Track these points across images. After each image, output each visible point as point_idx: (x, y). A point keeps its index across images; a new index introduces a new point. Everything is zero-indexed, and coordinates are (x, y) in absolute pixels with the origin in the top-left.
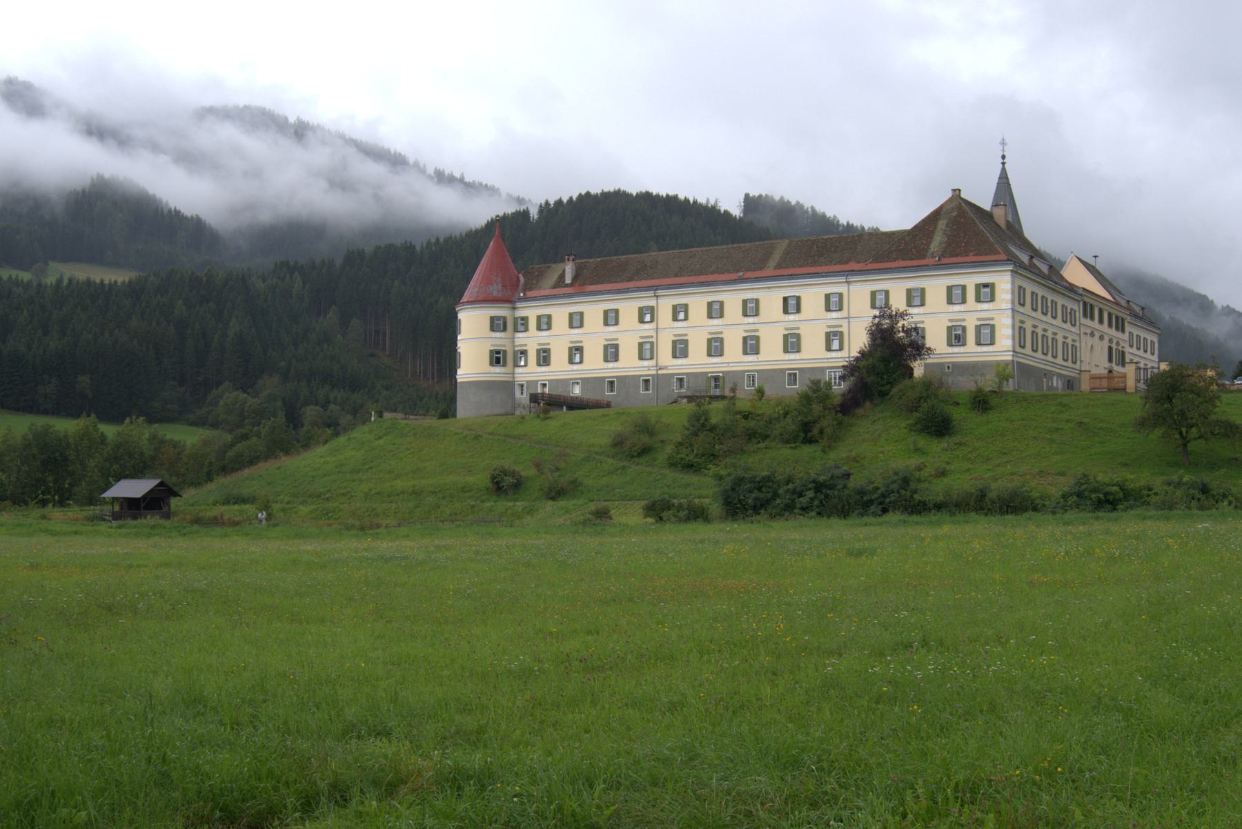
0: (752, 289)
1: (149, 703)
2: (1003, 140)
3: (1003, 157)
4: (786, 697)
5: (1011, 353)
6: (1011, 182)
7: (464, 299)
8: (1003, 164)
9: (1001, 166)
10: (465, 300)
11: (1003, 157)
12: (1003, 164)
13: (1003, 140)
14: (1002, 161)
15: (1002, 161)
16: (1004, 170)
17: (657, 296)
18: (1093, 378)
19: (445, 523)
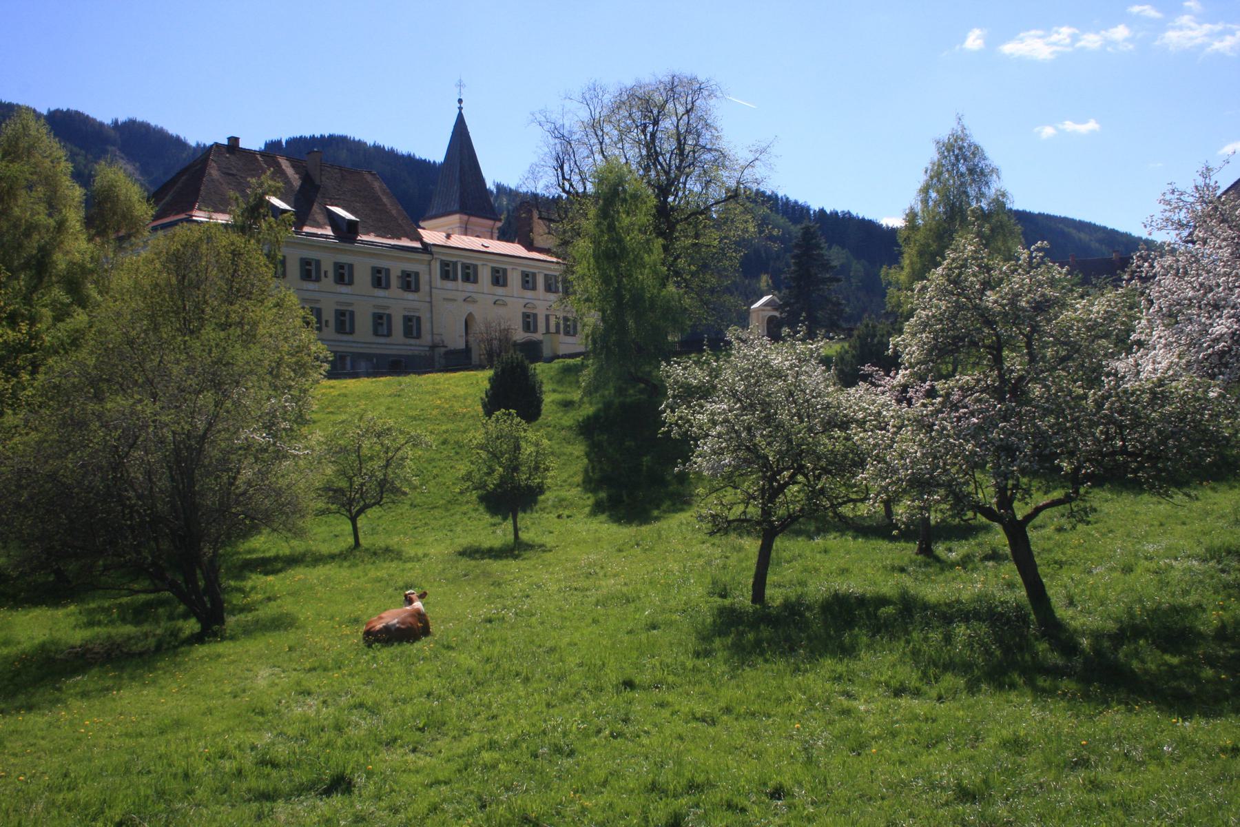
2: (460, 81)
3: (460, 101)
11: (460, 101)
13: (460, 81)
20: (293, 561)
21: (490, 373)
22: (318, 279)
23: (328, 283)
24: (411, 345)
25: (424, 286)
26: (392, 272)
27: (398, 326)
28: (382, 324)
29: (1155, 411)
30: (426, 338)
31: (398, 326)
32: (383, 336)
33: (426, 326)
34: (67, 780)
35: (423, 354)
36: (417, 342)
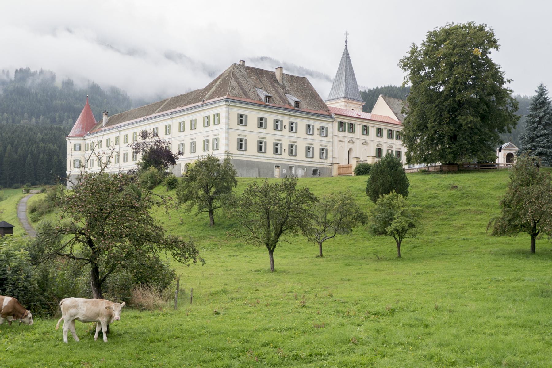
0: (178, 117)
1: (254, 262)
2: (347, 32)
3: (346, 42)
4: (162, 221)
5: (224, 154)
6: (350, 56)
7: (70, 134)
8: (346, 46)
9: (345, 47)
10: (71, 135)
11: (346, 42)
12: (346, 46)
13: (347, 32)
14: (345, 44)
15: (345, 44)
16: (346, 49)
17: (85, 139)
18: (340, 168)
19: (108, 166)
20: (504, 243)
21: (369, 177)
22: (281, 130)
23: (286, 131)
24: (323, 163)
25: (330, 135)
26: (315, 127)
27: (385, 133)
28: (309, 152)
29: (547, 225)
30: (330, 160)
31: (385, 133)
32: (310, 158)
33: (330, 154)
34: (15, 277)
35: (328, 167)
36: (325, 161)
